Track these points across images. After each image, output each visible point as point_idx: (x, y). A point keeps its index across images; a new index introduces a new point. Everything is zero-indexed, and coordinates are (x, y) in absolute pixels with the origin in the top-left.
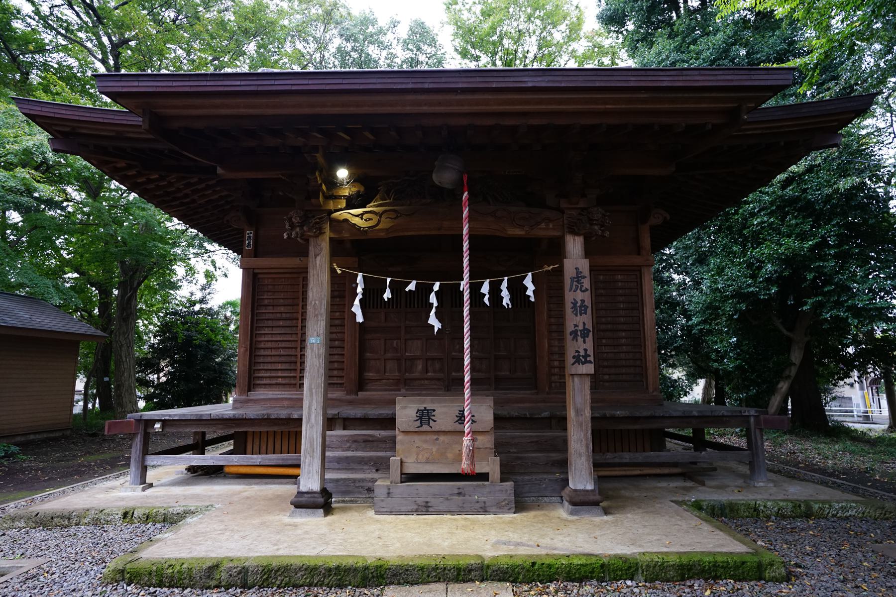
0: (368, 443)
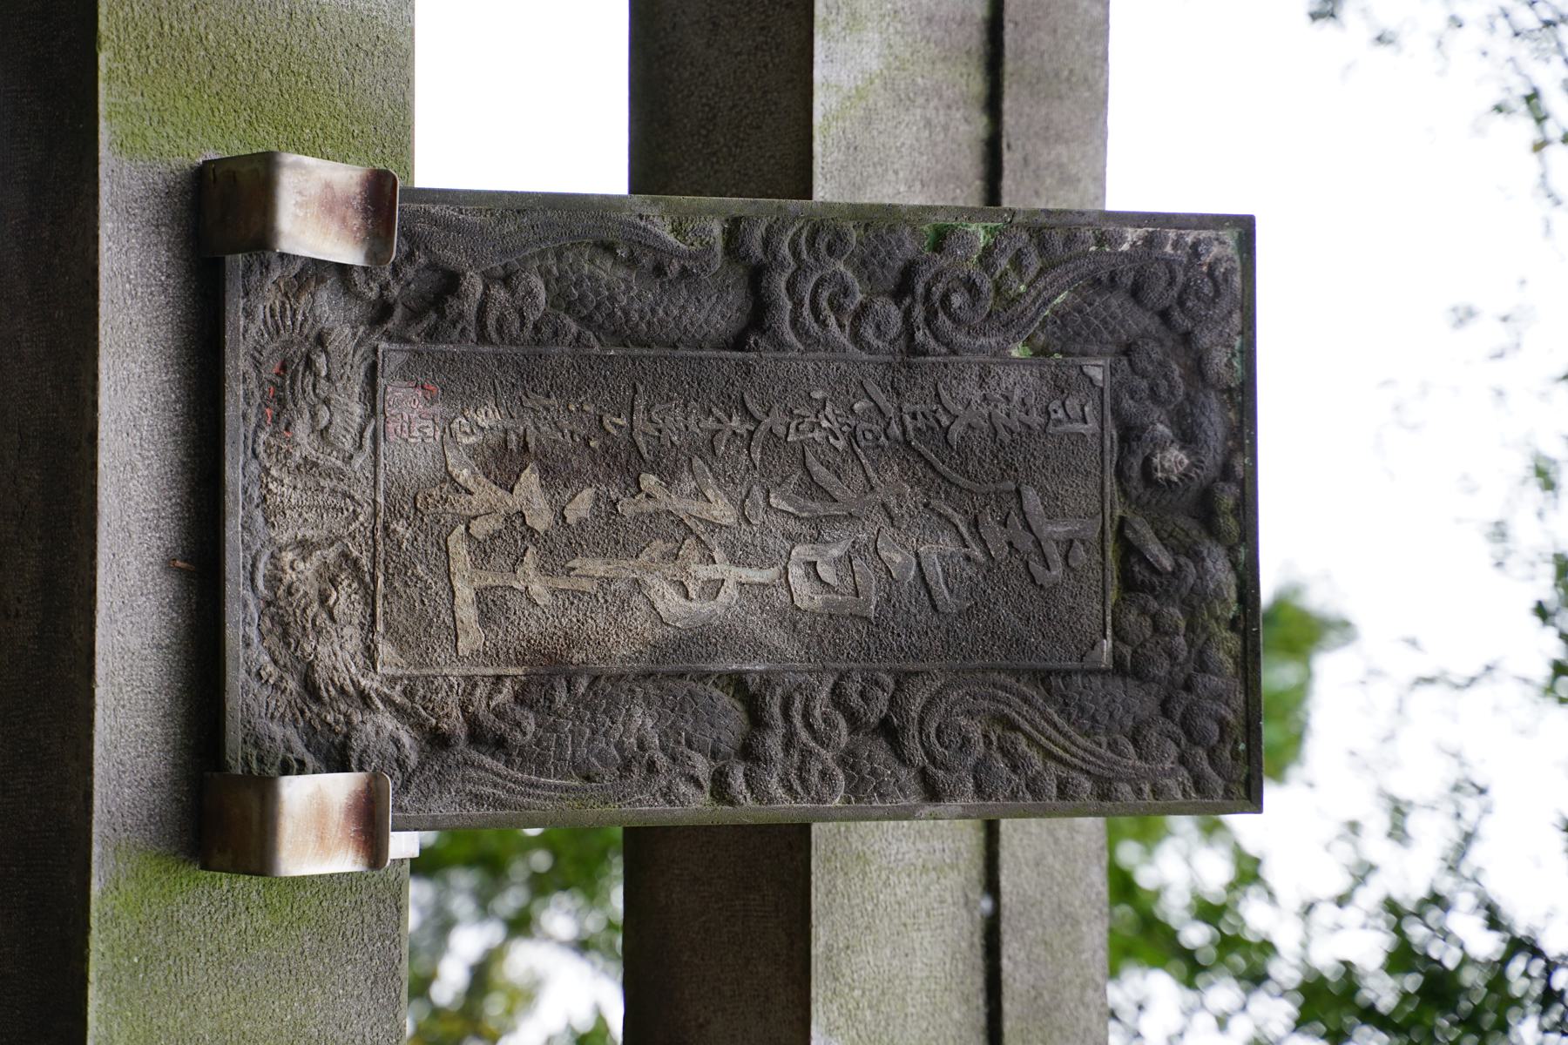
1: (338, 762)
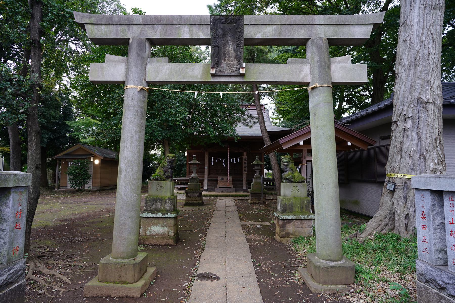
0: (213, 183)
1: (240, 69)
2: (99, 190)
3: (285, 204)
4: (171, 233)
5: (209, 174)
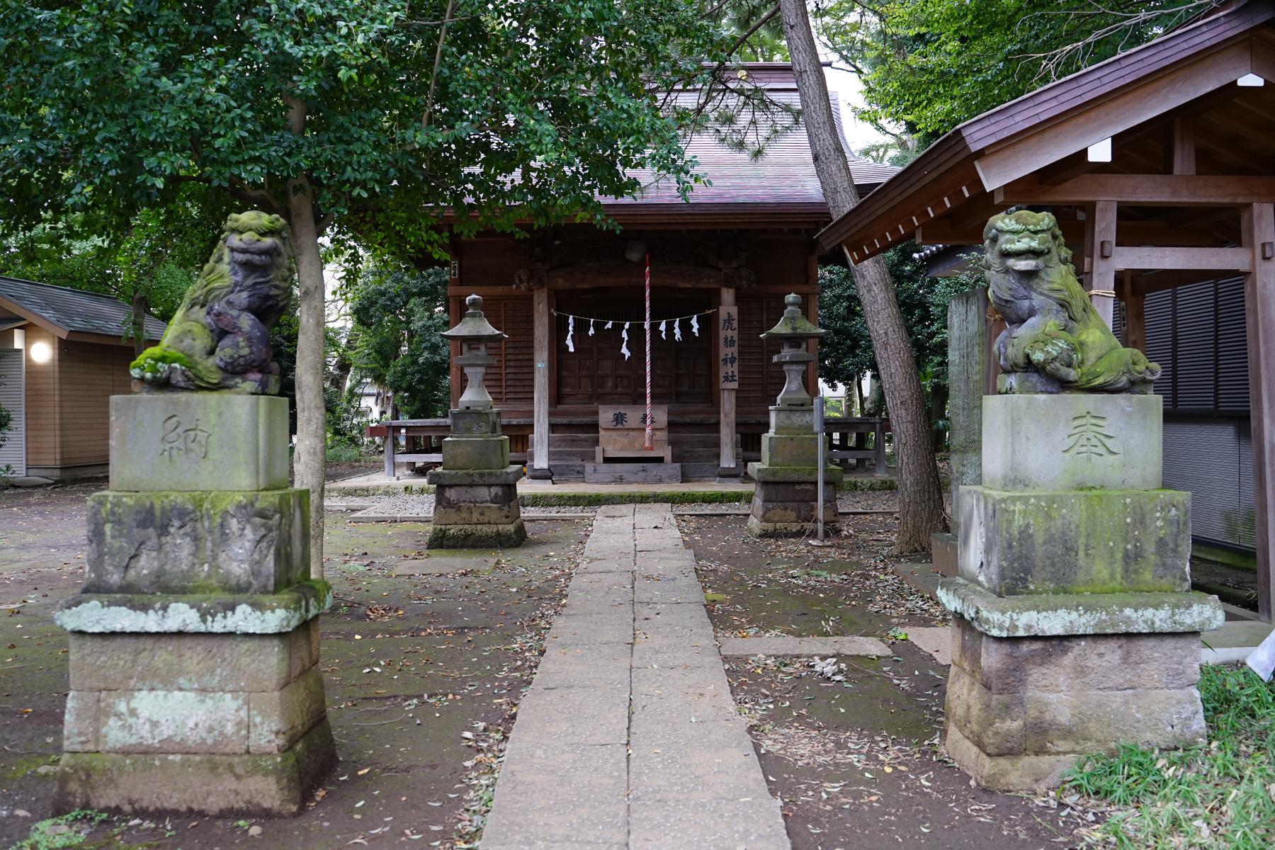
2: (56, 482)
3: (1025, 535)
4: (267, 733)
5: (557, 398)
